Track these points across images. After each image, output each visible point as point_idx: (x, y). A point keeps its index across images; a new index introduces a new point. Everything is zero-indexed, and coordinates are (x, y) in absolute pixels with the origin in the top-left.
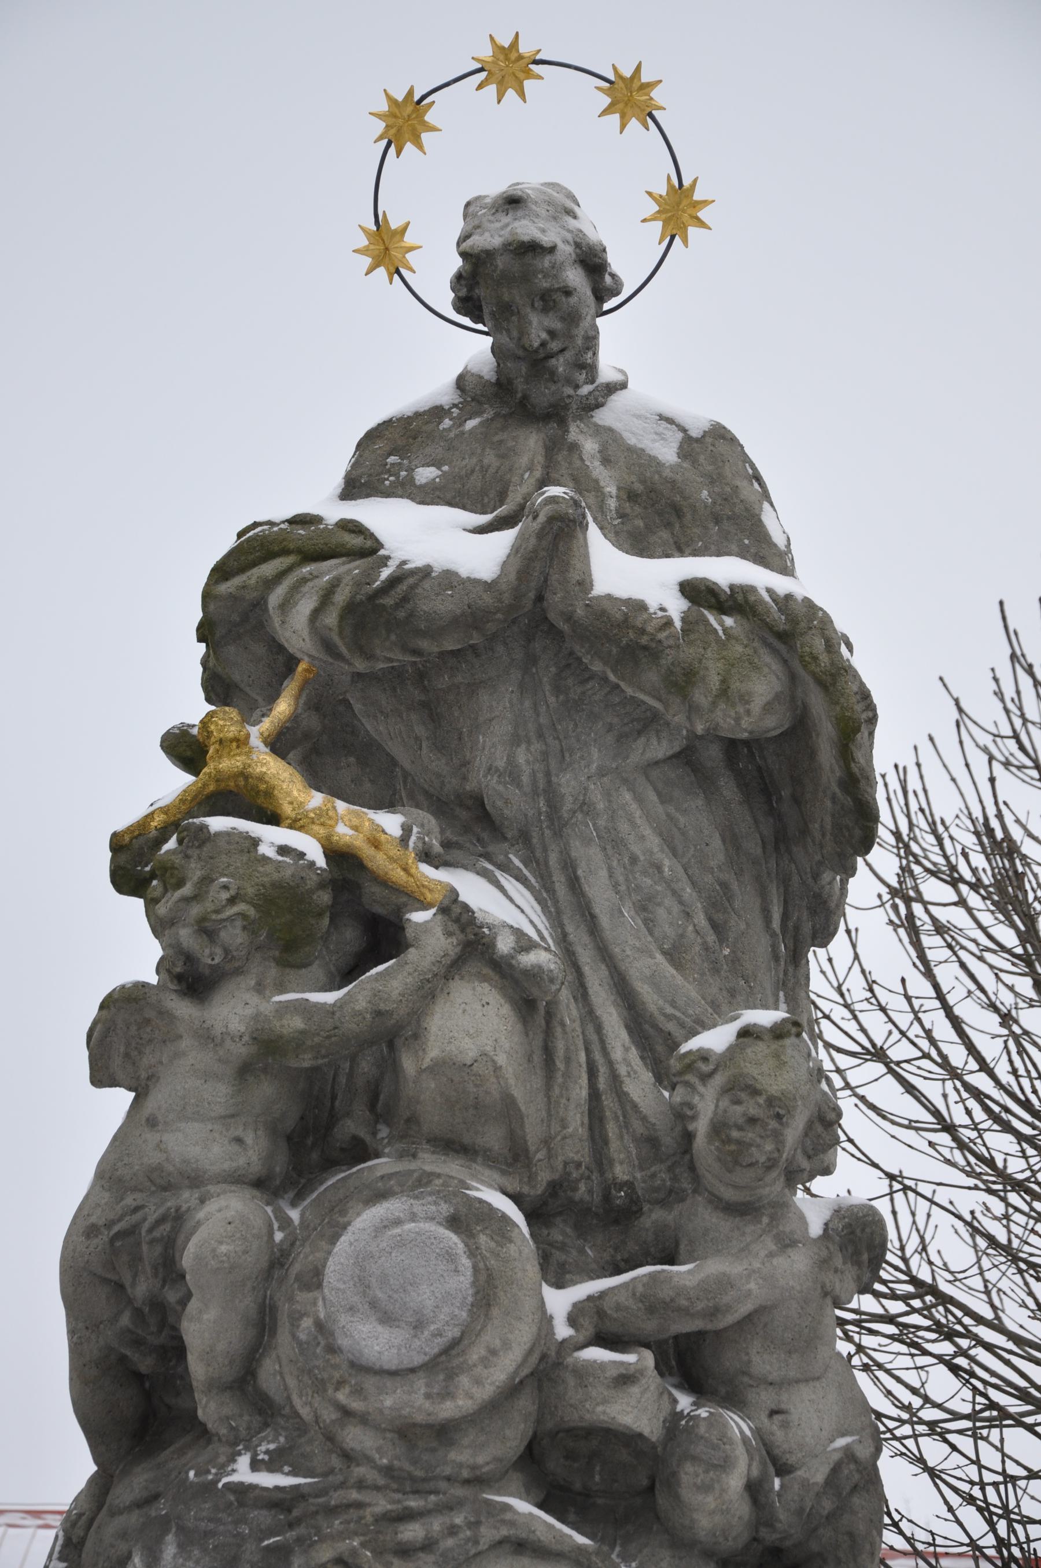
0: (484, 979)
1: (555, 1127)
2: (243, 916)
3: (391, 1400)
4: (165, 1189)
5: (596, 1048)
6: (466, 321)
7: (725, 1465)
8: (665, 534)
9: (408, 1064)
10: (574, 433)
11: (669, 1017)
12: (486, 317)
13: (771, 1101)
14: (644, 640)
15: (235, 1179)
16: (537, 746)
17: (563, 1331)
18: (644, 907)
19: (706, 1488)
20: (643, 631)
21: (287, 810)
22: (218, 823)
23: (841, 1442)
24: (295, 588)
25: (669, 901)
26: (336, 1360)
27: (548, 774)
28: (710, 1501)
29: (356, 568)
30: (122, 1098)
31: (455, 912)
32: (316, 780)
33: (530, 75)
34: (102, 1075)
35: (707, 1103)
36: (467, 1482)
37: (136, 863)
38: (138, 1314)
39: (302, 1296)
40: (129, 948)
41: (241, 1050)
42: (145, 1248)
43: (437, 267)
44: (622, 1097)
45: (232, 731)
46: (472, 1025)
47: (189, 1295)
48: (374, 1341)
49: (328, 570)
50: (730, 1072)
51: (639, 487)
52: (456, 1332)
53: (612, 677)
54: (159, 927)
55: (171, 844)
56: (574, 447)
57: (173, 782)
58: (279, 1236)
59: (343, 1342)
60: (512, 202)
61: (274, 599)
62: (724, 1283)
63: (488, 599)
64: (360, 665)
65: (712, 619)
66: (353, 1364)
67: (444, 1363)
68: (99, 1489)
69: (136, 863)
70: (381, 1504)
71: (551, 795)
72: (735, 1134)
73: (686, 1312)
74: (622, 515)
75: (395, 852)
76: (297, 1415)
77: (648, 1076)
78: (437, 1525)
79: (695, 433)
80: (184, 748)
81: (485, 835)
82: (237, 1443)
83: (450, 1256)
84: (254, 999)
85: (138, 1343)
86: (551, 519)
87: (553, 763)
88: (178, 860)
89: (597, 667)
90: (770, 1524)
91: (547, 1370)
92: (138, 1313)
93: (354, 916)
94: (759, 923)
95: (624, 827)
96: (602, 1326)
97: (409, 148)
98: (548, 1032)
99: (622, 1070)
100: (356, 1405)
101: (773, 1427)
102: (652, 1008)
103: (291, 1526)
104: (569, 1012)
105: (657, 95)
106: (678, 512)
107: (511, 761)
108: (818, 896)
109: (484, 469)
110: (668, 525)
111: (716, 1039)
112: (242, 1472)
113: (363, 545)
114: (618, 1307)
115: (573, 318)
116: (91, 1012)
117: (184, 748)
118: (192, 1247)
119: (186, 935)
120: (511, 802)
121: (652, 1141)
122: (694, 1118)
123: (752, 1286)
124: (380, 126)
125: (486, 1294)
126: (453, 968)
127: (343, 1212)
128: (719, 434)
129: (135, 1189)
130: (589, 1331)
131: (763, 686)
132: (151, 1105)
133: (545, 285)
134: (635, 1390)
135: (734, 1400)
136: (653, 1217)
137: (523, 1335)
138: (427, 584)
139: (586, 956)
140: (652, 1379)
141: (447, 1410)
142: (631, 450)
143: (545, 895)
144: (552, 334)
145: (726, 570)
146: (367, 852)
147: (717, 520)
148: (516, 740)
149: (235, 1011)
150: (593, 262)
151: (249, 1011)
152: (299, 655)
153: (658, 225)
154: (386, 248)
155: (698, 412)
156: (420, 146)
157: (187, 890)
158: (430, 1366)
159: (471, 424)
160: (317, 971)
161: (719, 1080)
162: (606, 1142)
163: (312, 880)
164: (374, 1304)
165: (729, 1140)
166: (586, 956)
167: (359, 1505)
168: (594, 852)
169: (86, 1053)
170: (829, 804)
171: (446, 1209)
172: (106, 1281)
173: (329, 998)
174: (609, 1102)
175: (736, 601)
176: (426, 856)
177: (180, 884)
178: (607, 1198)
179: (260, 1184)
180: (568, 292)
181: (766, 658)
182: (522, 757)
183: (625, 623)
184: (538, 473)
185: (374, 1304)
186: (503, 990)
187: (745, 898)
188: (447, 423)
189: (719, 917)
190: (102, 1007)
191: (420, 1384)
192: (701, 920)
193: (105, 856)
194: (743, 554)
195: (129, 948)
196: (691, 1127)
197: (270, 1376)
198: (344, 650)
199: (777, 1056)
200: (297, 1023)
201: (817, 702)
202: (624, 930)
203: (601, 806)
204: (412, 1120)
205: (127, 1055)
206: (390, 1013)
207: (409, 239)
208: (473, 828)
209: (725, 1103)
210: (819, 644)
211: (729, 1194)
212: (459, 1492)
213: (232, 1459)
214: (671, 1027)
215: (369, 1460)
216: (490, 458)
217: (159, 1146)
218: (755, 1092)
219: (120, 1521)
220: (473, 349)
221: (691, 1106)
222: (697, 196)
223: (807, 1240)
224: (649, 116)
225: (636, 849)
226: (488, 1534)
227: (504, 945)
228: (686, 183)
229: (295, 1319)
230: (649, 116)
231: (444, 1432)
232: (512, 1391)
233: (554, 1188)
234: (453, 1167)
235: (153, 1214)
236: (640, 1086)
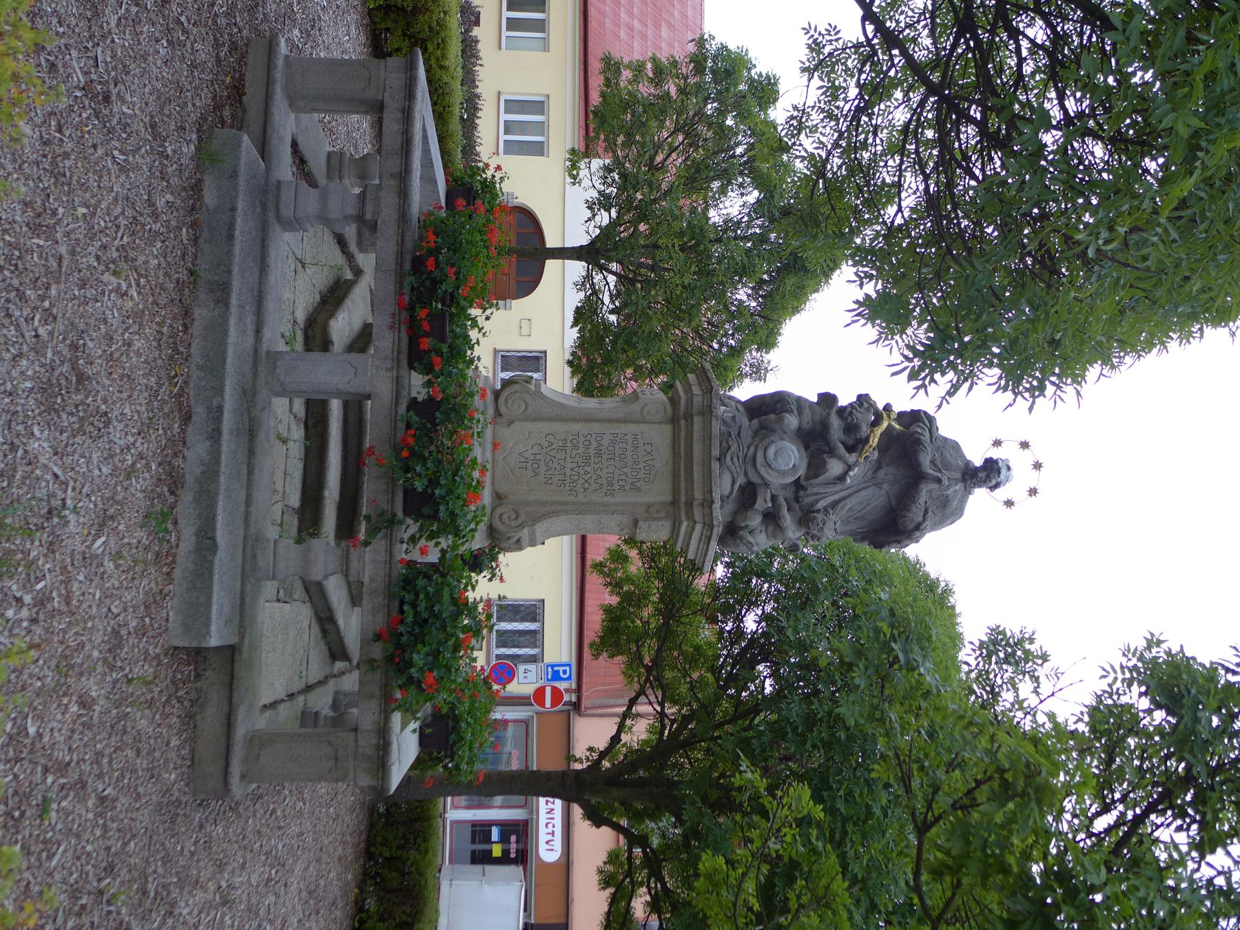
18: (860, 503)
34: (820, 395)
37: (863, 399)
43: (995, 454)
48: (771, 451)
54: (851, 405)
57: (880, 406)
60: (1009, 468)
68: (739, 401)
69: (863, 399)
80: (888, 408)
104: (839, 487)
115: (985, 482)
117: (888, 408)
126: (846, 463)
139: (849, 491)
141: (758, 465)
150: (997, 486)
154: (997, 443)
166: (849, 491)
193: (864, 392)
220: (978, 462)
232: (763, 479)
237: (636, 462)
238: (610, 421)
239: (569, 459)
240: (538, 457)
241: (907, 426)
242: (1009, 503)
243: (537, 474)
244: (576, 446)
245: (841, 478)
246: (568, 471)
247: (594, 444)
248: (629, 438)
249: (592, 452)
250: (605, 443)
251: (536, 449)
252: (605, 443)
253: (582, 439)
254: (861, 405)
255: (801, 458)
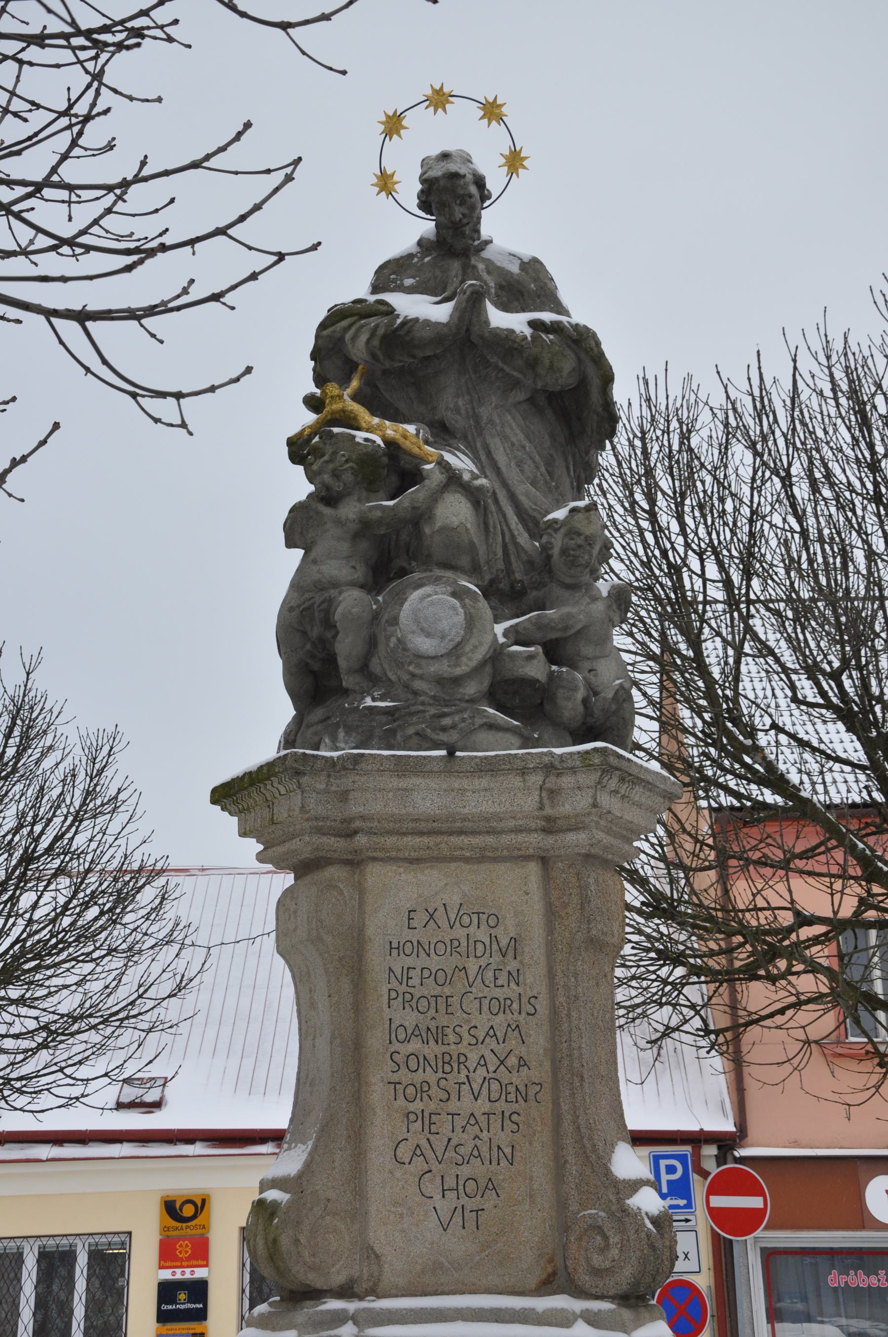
0: (456, 492)
1: (492, 555)
2: (352, 468)
3: (433, 668)
4: (322, 590)
5: (503, 524)
6: (423, 214)
7: (575, 689)
8: (516, 304)
9: (427, 530)
10: (473, 261)
11: (534, 510)
12: (434, 211)
13: (587, 538)
14: (516, 345)
15: (353, 584)
16: (467, 397)
17: (501, 640)
18: (519, 464)
19: (568, 699)
20: (515, 342)
21: (364, 425)
22: (336, 430)
23: (618, 682)
24: (358, 330)
25: (529, 462)
26: (407, 654)
27: (473, 409)
28: (570, 705)
29: (385, 320)
30: (299, 553)
31: (442, 464)
32: (373, 413)
33: (448, 102)
34: (290, 543)
35: (558, 541)
36: (467, 701)
37: (299, 450)
38: (314, 644)
39: (390, 629)
40: (298, 486)
41: (354, 527)
42: (317, 614)
43: (410, 189)
44: (516, 544)
45: (336, 392)
46: (455, 511)
47: (338, 632)
48: (424, 645)
49: (373, 322)
50: (568, 528)
51: (504, 283)
52: (459, 639)
53: (500, 364)
55: (317, 439)
56: (474, 267)
58: (374, 607)
59: (410, 646)
60: (445, 156)
61: (348, 336)
62: (570, 616)
63: (446, 330)
64: (387, 364)
65: (543, 336)
66: (414, 655)
67: (455, 652)
69: (299, 450)
70: (433, 711)
71: (477, 418)
72: (572, 552)
73: (553, 629)
74: (497, 296)
75: (414, 440)
76: (389, 680)
77: (526, 535)
78: (457, 718)
79: (526, 260)
81: (447, 437)
82: (363, 694)
83: (454, 608)
84: (358, 505)
85: (313, 657)
86: (472, 293)
87: (475, 405)
88: (321, 445)
89: (494, 360)
90: (592, 715)
91: (497, 655)
92: (313, 644)
93: (395, 469)
94: (565, 473)
95: (508, 430)
96: (517, 636)
97: (395, 137)
98: (485, 516)
99: (516, 533)
100: (418, 672)
101: (591, 676)
102: (527, 507)
103: (395, 721)
105: (504, 110)
106: (522, 293)
107: (456, 404)
108: (587, 462)
109: (435, 278)
110: (517, 300)
111: (560, 514)
112: (369, 702)
113: (389, 311)
114: (525, 629)
116: (285, 514)
117: (313, 403)
118: (339, 610)
119: (327, 478)
120: (458, 422)
121: (531, 562)
122: (552, 548)
123: (581, 617)
124: (382, 127)
125: (471, 622)
126: (444, 488)
127: (404, 594)
128: (535, 261)
129: (308, 591)
130: (512, 639)
131: (568, 364)
132: (313, 554)
133: (462, 192)
134: (535, 661)
135: (573, 666)
136: (533, 594)
137: (488, 639)
138: (418, 325)
140: (542, 657)
141: (458, 671)
142: (498, 267)
143: (476, 459)
144: (464, 215)
145: (547, 316)
146: (401, 441)
147: (539, 297)
148: (458, 396)
149: (350, 510)
150: (480, 182)
151: (357, 510)
152: (360, 361)
153: (506, 168)
154: (385, 183)
155: (527, 251)
156: (400, 136)
157: (326, 458)
158: (448, 654)
159: (427, 259)
160: (381, 494)
161: (563, 531)
162: (511, 564)
163: (380, 453)
164: (422, 630)
165: (569, 555)
167: (424, 712)
168: (497, 440)
169: (283, 534)
170: (595, 417)
171: (450, 589)
172: (298, 630)
173: (391, 503)
174: (511, 547)
175: (555, 328)
176: (427, 442)
177: (323, 455)
178: (512, 587)
179: (362, 587)
180: (471, 196)
181: (568, 352)
182: (461, 402)
183: (507, 338)
184: (460, 278)
185: (422, 630)
186: (466, 496)
187: (560, 463)
188: (416, 260)
189: (550, 469)
190: (290, 512)
191: (445, 662)
192: (543, 469)
194: (551, 310)
195: (298, 486)
196: (550, 552)
197: (375, 666)
198: (381, 357)
199: (588, 518)
200: (378, 514)
201: (591, 370)
202: (512, 475)
203: (498, 421)
204: (429, 556)
205: (302, 533)
206: (418, 508)
207: (395, 178)
208: (442, 433)
209: (566, 540)
210: (593, 343)
211: (568, 580)
212: (465, 705)
213: (363, 698)
214: (535, 514)
215: (425, 693)
216: (438, 273)
217: (318, 571)
218: (579, 534)
219: (312, 730)
220: (426, 226)
221: (551, 543)
222: (522, 155)
223: (601, 598)
224: (500, 119)
225: (514, 440)
226: (479, 721)
227: (466, 477)
228: (518, 149)
229: (388, 639)
230: (500, 119)
231: (457, 681)
232: (483, 663)
233: (492, 582)
234: (449, 574)
235: (318, 599)
236: (523, 538)
237: (454, 946)
238: (358, 1008)
239: (453, 1106)
240: (450, 1182)
241: (349, 368)
242: (514, 161)
243: (491, 1185)
244: (422, 1090)
245: (474, 495)
246: (482, 1104)
247: (415, 1045)
248: (399, 963)
249: (432, 1050)
250: (410, 1019)
251: (432, 1187)
252: (410, 1019)
253: (404, 1076)
254: (317, 452)
255: (437, 580)
